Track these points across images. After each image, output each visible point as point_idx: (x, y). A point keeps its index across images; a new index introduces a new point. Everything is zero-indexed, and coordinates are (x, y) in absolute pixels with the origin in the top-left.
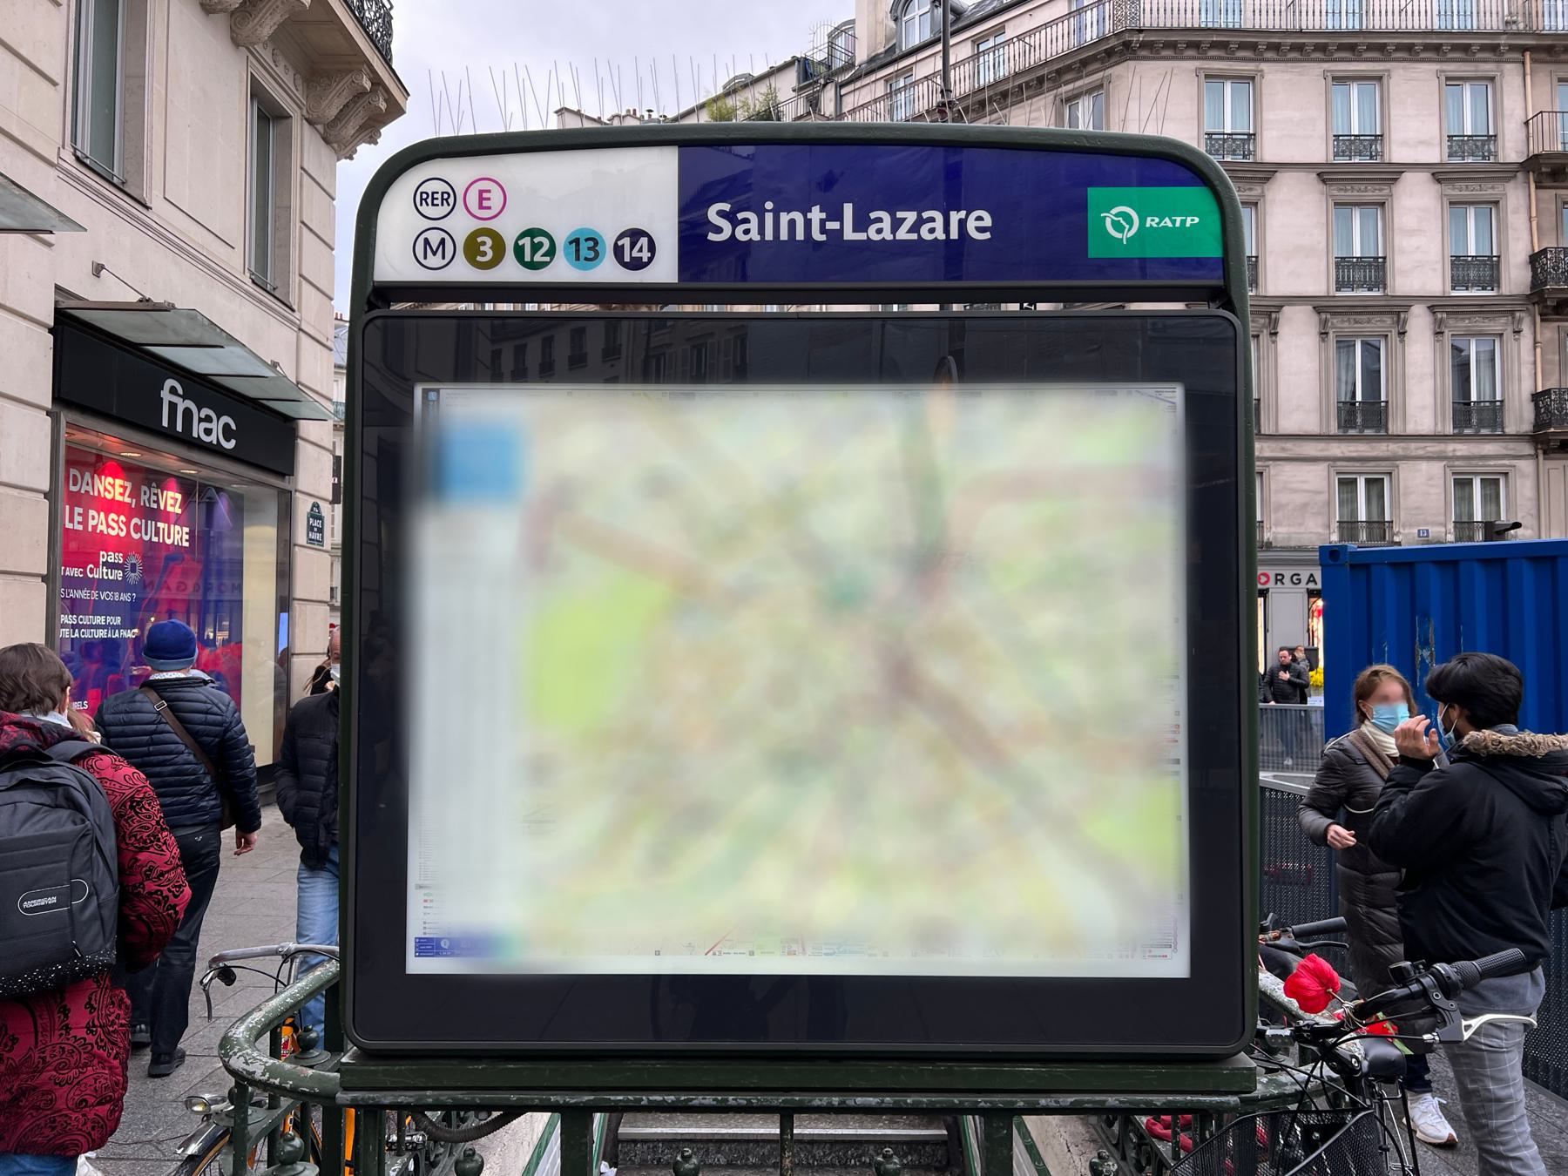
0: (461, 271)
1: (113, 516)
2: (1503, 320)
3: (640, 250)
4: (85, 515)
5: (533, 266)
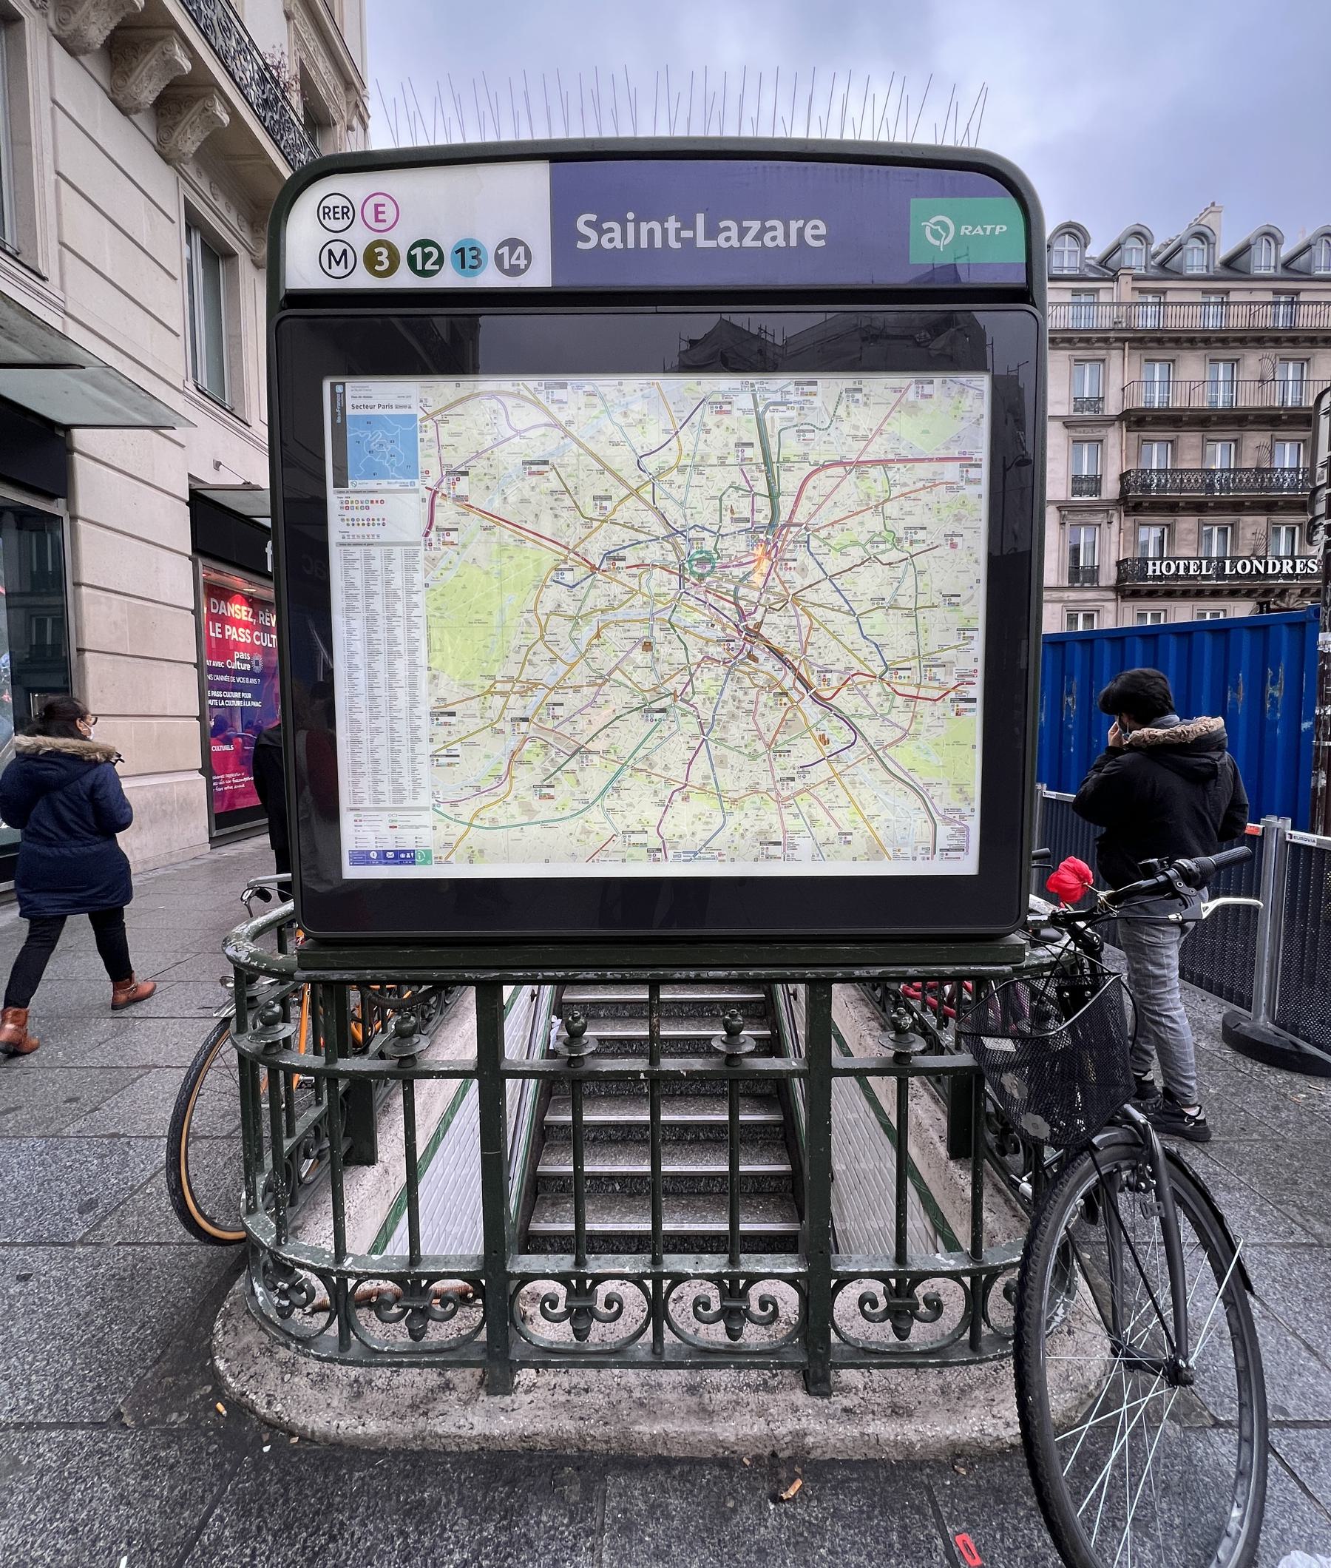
0: (362, 280)
1: (241, 630)
3: (518, 258)
4: (223, 628)
5: (425, 274)
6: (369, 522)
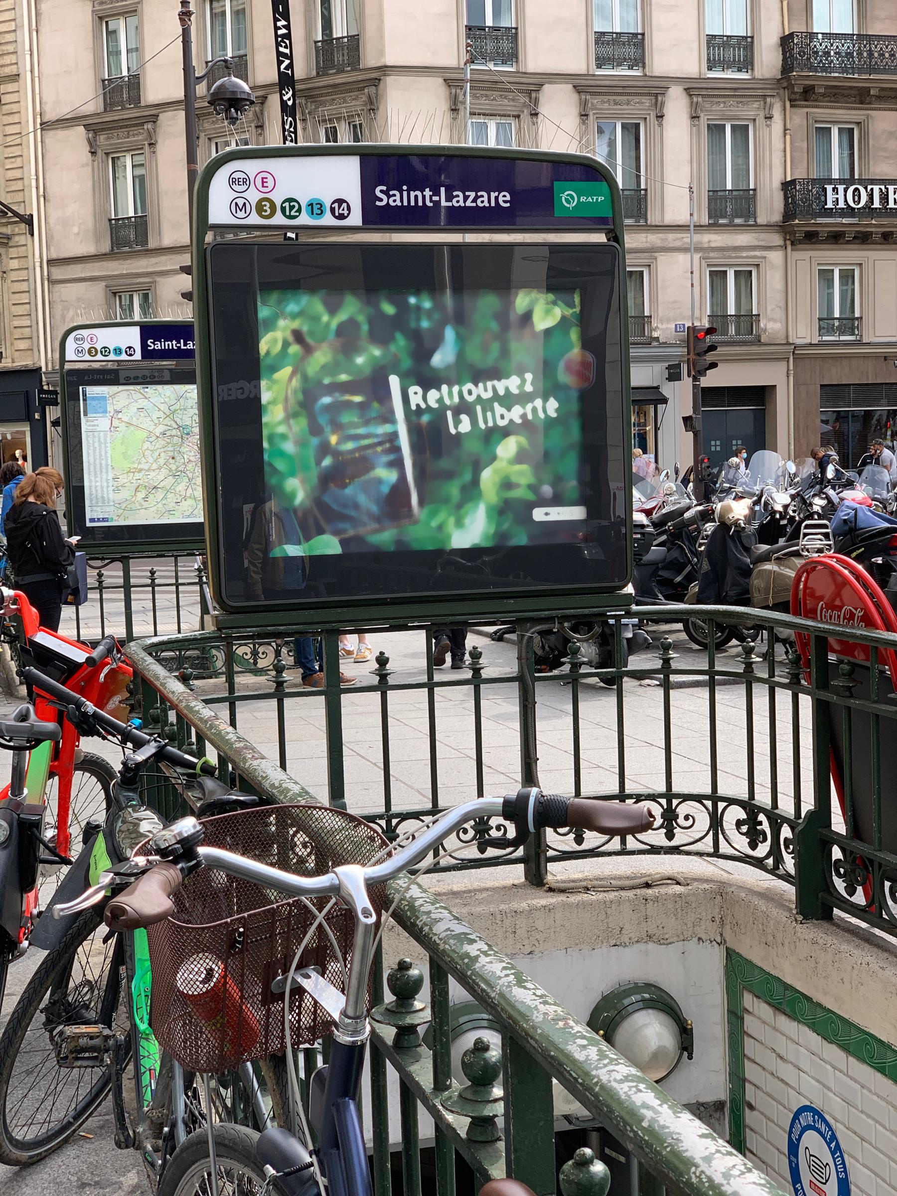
0: (254, 219)
2: (755, 105)
5: (105, 356)
6: (94, 425)
